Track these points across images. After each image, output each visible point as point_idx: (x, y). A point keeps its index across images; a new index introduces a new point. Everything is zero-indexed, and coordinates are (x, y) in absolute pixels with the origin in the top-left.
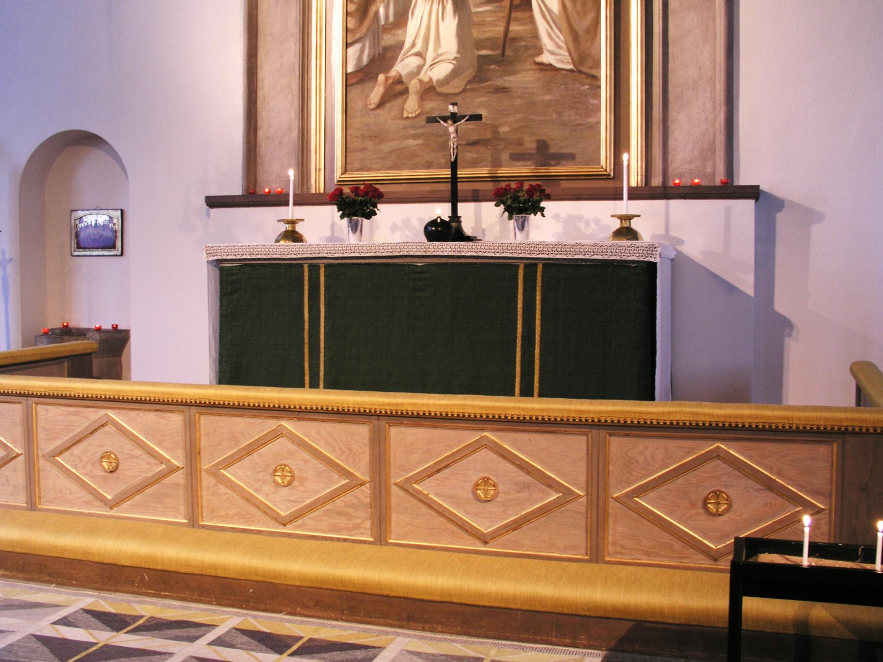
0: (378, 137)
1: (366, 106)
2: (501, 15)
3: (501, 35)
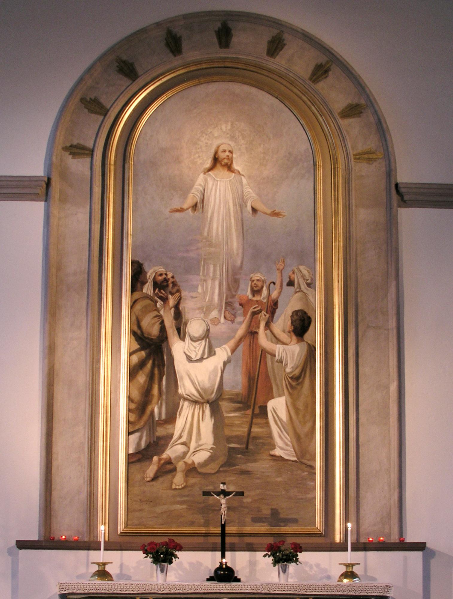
0: (153, 501)
1: (144, 479)
2: (245, 420)
3: (246, 434)
